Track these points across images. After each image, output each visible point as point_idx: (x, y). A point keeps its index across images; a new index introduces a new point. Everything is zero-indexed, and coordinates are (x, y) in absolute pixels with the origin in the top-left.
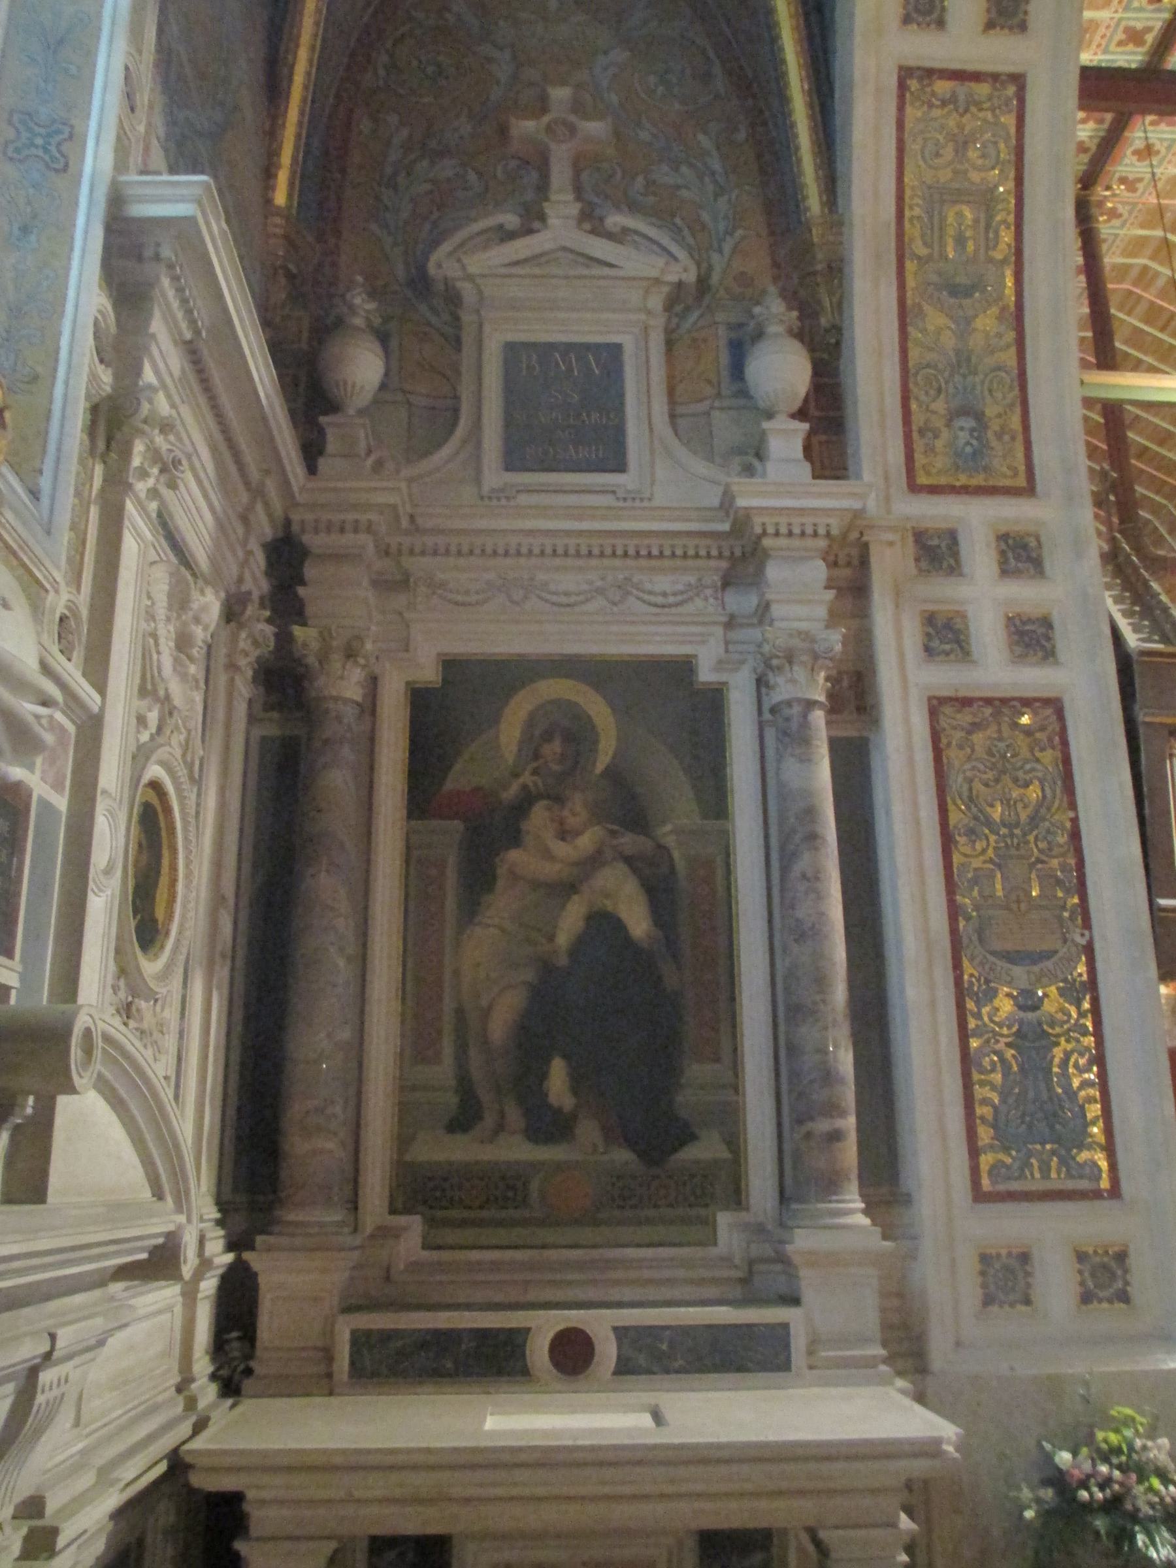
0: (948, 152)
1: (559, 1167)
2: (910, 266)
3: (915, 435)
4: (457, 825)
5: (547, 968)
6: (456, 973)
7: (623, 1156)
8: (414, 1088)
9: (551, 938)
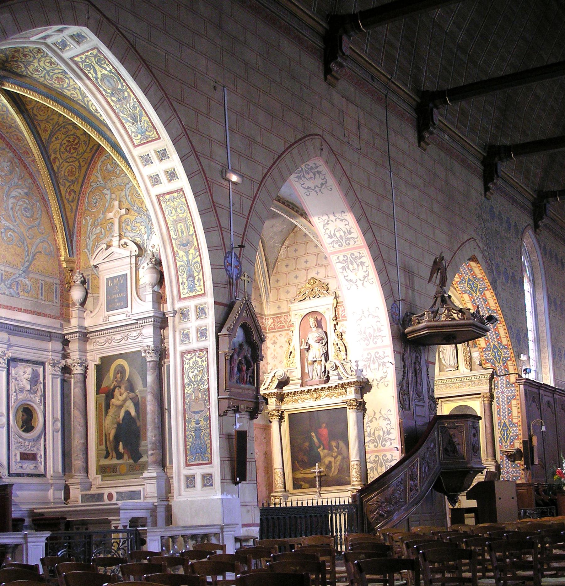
0: (174, 212)
1: (122, 464)
2: (173, 242)
3: (180, 284)
4: (104, 395)
5: (119, 424)
6: (105, 427)
7: (131, 461)
8: (99, 450)
9: (119, 417)
